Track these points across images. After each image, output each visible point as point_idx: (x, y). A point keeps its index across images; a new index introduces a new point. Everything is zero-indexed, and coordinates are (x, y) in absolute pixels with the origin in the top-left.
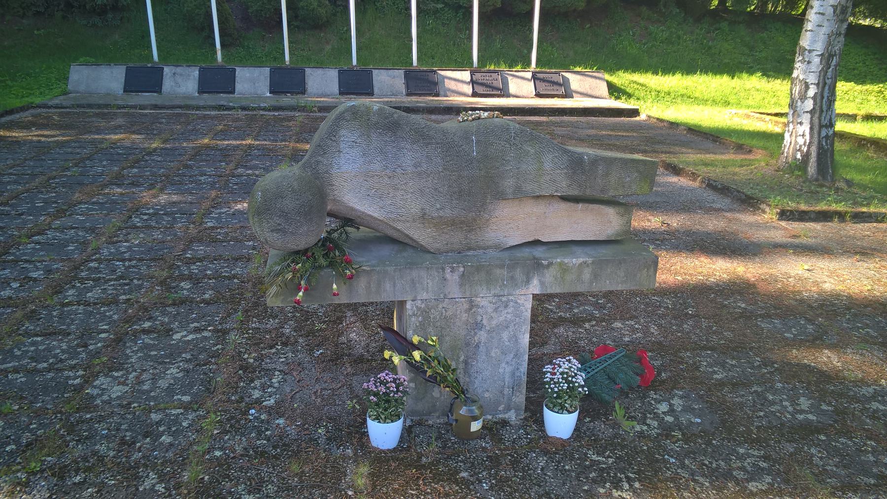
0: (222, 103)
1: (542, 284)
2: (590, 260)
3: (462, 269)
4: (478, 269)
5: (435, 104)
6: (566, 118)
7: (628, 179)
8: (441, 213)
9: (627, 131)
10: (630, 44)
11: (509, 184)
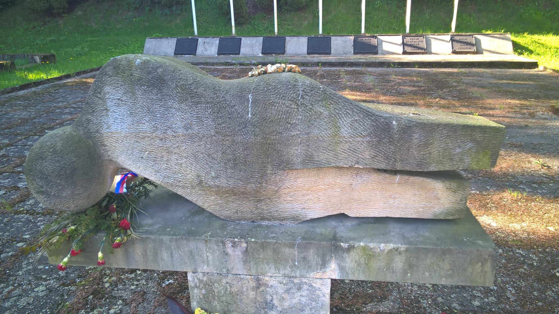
0: (230, 61)
1: (342, 269)
2: (403, 247)
3: (244, 245)
4: (264, 246)
5: (373, 60)
6: (474, 70)
7: (458, 150)
8: (217, 182)
9: (525, 80)
10: (535, 12)
11: (296, 152)
